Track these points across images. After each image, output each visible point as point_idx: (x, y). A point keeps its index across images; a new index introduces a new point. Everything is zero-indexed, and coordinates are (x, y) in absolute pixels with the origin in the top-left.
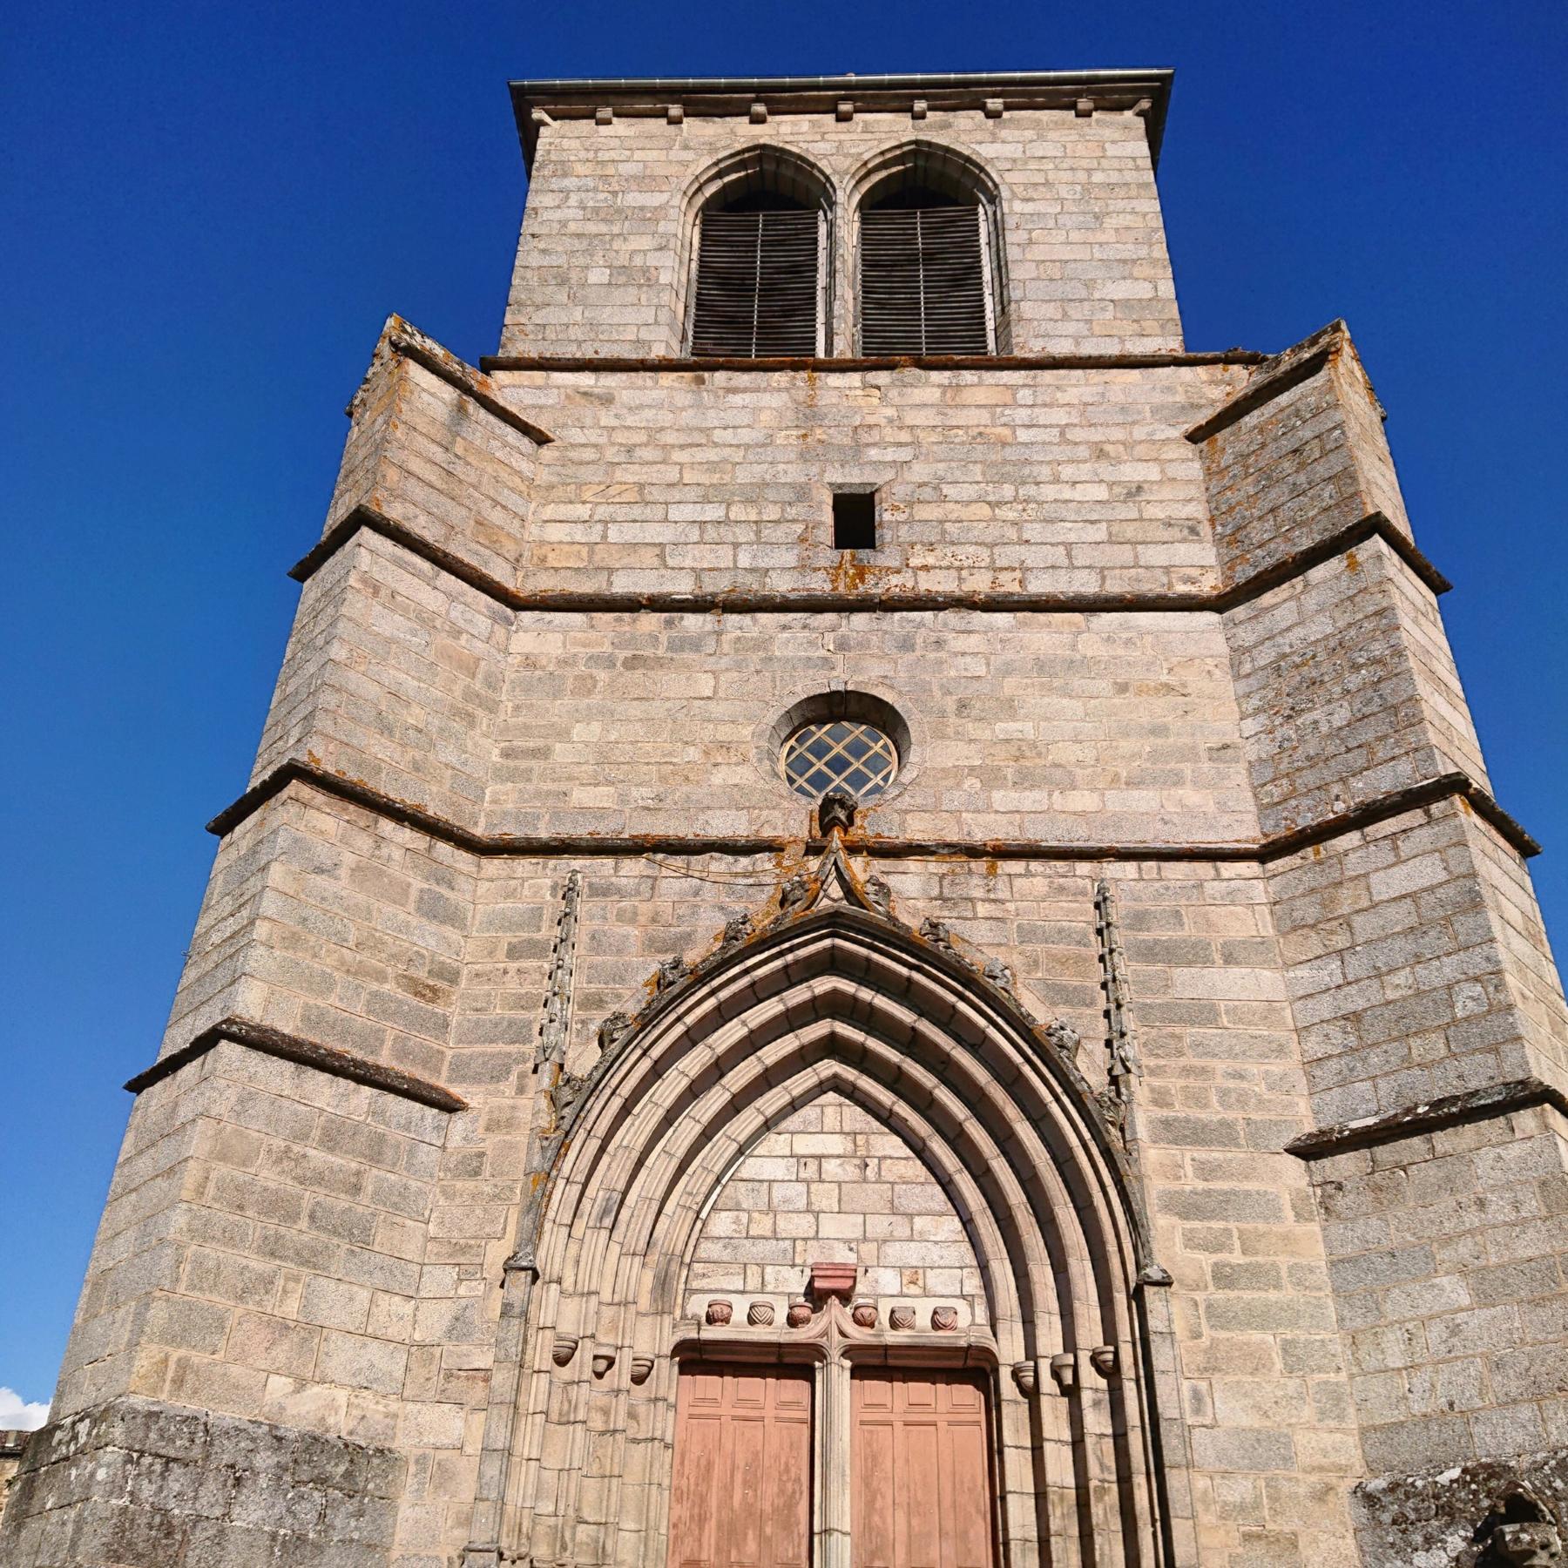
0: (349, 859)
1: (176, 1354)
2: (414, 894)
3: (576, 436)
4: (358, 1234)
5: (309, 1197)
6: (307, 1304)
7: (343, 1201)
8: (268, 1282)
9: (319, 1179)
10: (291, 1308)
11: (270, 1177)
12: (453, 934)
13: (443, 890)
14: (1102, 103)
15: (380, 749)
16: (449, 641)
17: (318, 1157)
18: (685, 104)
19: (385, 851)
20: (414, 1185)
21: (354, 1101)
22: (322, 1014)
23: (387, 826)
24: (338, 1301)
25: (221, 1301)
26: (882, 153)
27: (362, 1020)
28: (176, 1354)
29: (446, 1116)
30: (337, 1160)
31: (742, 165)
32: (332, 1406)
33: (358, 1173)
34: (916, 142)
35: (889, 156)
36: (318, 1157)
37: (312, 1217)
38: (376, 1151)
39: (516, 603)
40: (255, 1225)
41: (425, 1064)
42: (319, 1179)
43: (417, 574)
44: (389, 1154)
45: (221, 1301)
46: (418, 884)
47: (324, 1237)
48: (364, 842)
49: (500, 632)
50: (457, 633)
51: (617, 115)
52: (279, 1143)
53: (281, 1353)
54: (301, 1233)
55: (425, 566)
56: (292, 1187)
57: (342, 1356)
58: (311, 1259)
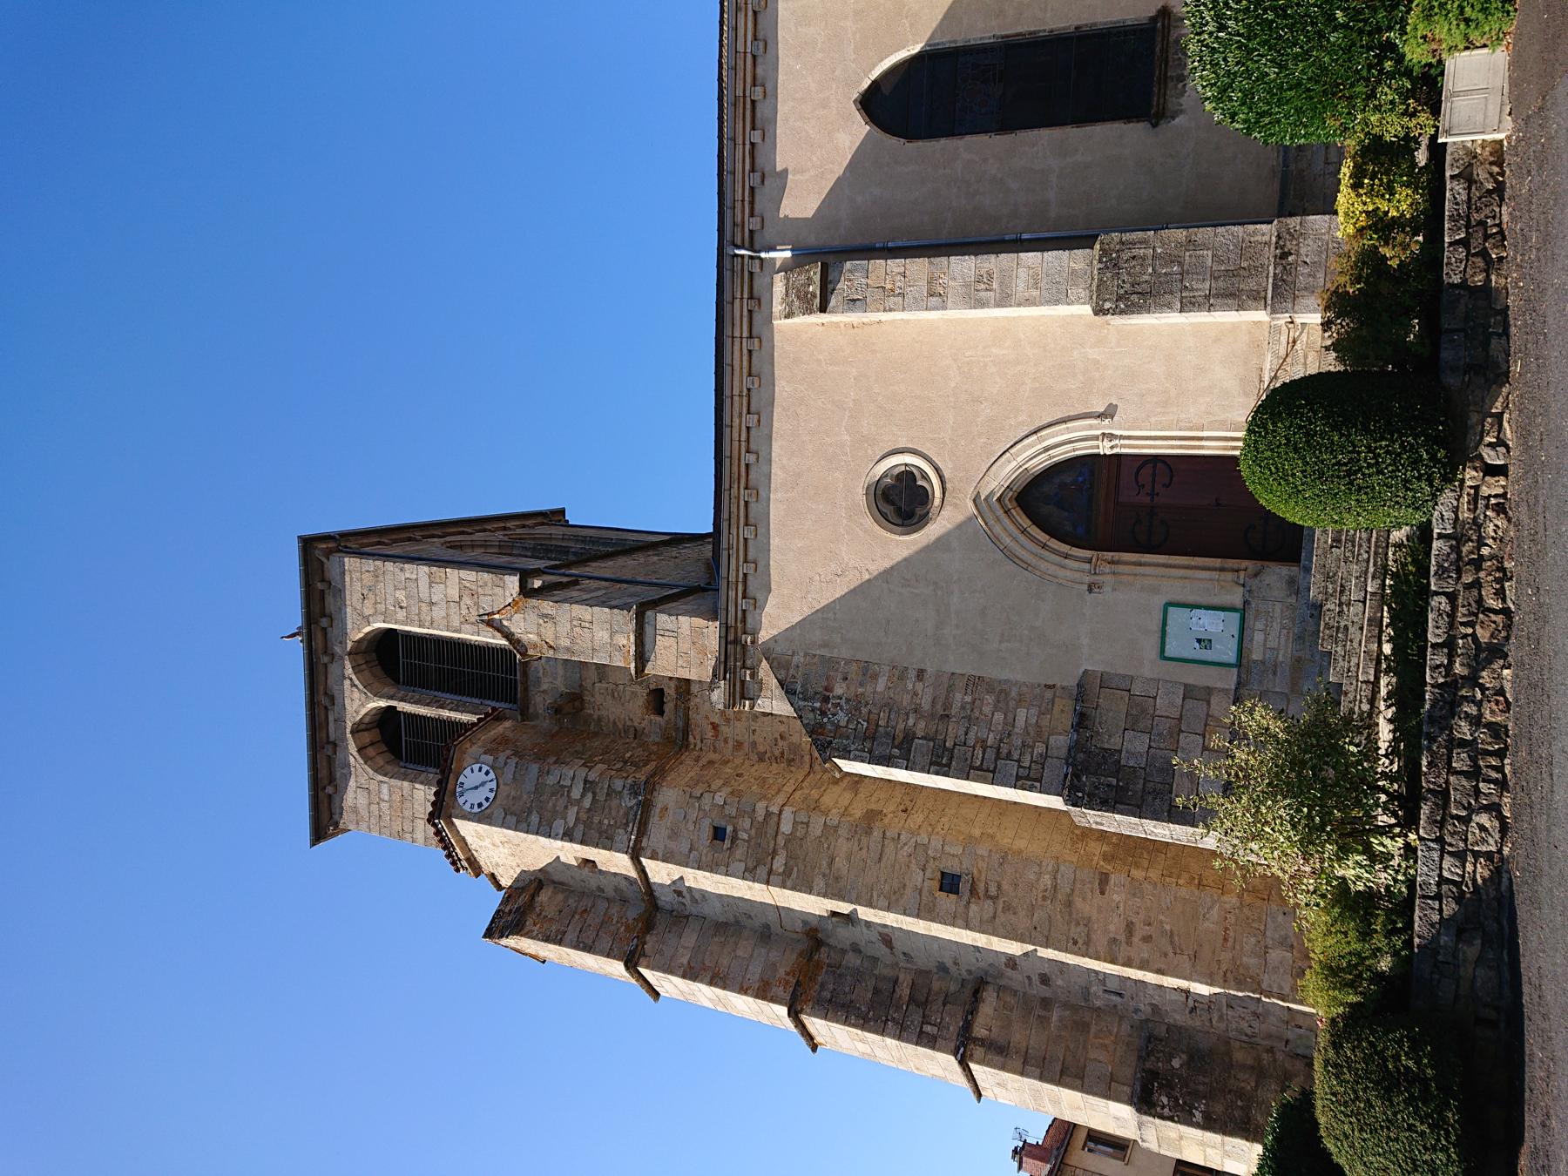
2: (1043, 1013)
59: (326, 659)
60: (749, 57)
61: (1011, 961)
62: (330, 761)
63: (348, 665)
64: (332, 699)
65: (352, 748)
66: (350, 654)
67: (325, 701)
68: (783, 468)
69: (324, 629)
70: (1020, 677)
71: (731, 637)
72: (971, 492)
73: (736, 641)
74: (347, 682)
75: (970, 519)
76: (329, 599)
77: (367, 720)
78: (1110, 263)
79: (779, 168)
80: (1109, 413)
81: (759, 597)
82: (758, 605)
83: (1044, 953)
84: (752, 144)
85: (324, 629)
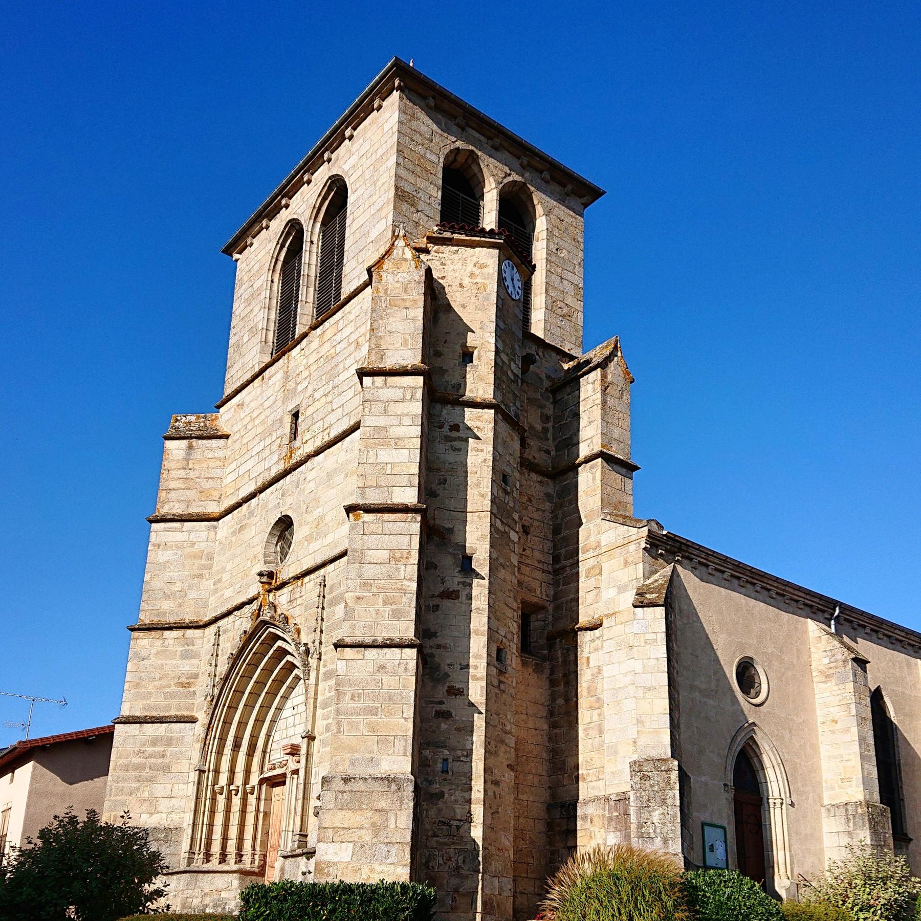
0: (154, 651)
1: (113, 814)
2: (178, 653)
3: (236, 428)
4: (166, 769)
5: (149, 761)
6: (151, 792)
7: (160, 760)
8: (138, 789)
9: (151, 756)
10: (146, 794)
11: (136, 760)
12: (195, 661)
13: (191, 647)
14: (384, 96)
15: (166, 605)
16: (191, 549)
17: (150, 749)
18: (266, 216)
19: (166, 643)
20: (184, 749)
21: (160, 730)
22: (149, 705)
23: (167, 633)
24: (160, 789)
25: (124, 797)
26: (319, 195)
27: (164, 703)
28: (113, 814)
29: (193, 725)
30: (156, 749)
31: (288, 234)
32: (162, 819)
33: (164, 751)
34: (330, 178)
35: (323, 194)
36: (150, 749)
37: (150, 768)
38: (169, 742)
39: (217, 519)
40: (132, 774)
41: (188, 709)
42: (151, 756)
43: (176, 530)
44: (174, 742)
45: (124, 797)
46: (180, 649)
47: (155, 772)
48: (159, 643)
49: (212, 534)
50: (193, 545)
51: (254, 238)
52: (137, 749)
53: (144, 808)
54: (146, 773)
55: (177, 525)
56: (144, 761)
57: (163, 805)
58: (152, 780)
59: (525, 160)
60: (890, 634)
61: (460, 692)
62: (452, 117)
63: (519, 179)
64: (496, 149)
65: (460, 144)
66: (524, 184)
67: (497, 141)
68: (754, 606)
69: (541, 172)
70: (682, 736)
71: (684, 547)
72: (757, 722)
73: (680, 550)
74: (454, 139)
75: (746, 718)
76: (558, 188)
77: (474, 167)
78: (657, 762)
79: (858, 639)
80: (792, 805)
81: (697, 572)
82: (693, 569)
83: (479, 722)
84: (723, 572)
85: (541, 172)
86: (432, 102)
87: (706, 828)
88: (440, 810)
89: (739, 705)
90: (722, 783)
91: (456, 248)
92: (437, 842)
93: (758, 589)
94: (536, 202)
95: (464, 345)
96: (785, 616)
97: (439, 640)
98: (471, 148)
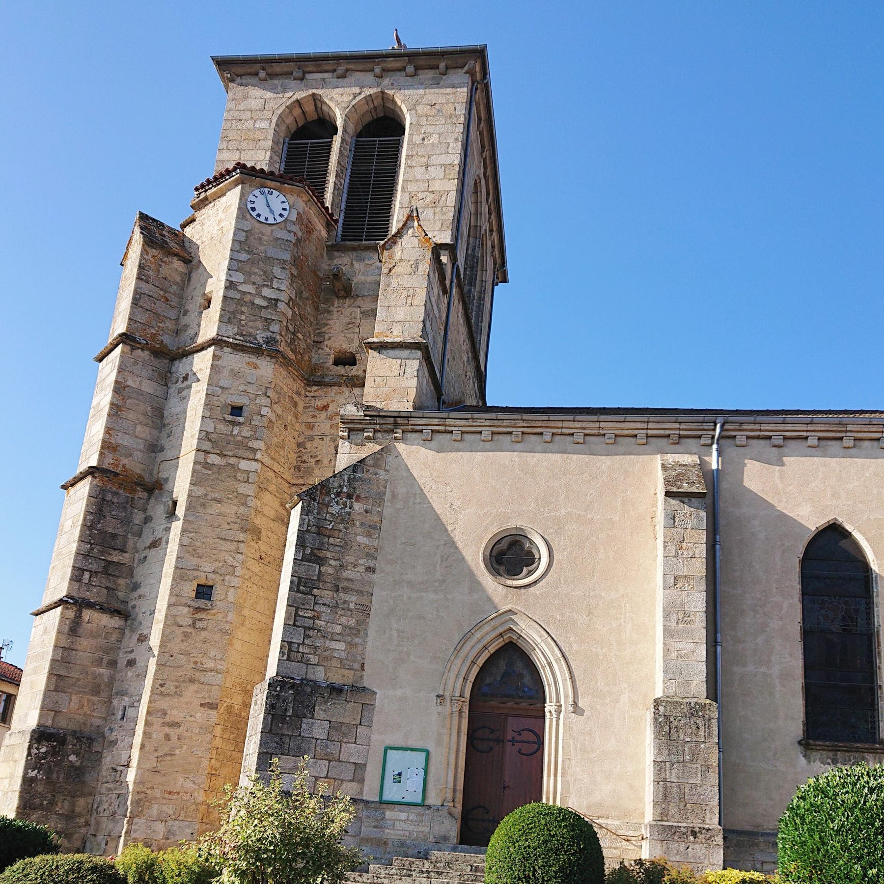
59: (378, 70)
61: (143, 639)
63: (373, 91)
64: (343, 76)
66: (383, 92)
67: (341, 69)
69: (404, 69)
71: (399, 421)
73: (396, 425)
78: (695, 711)
85: (404, 69)
86: (262, 74)
87: (424, 754)
88: (113, 756)
89: (483, 590)
90: (433, 695)
91: (212, 204)
92: (106, 788)
93: (777, 442)
94: (399, 103)
95: (204, 294)
96: (604, 463)
97: (140, 591)
98: (310, 92)
